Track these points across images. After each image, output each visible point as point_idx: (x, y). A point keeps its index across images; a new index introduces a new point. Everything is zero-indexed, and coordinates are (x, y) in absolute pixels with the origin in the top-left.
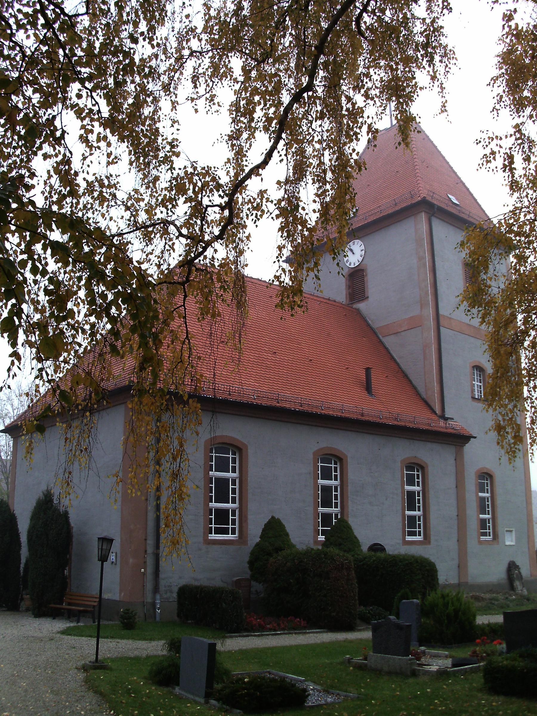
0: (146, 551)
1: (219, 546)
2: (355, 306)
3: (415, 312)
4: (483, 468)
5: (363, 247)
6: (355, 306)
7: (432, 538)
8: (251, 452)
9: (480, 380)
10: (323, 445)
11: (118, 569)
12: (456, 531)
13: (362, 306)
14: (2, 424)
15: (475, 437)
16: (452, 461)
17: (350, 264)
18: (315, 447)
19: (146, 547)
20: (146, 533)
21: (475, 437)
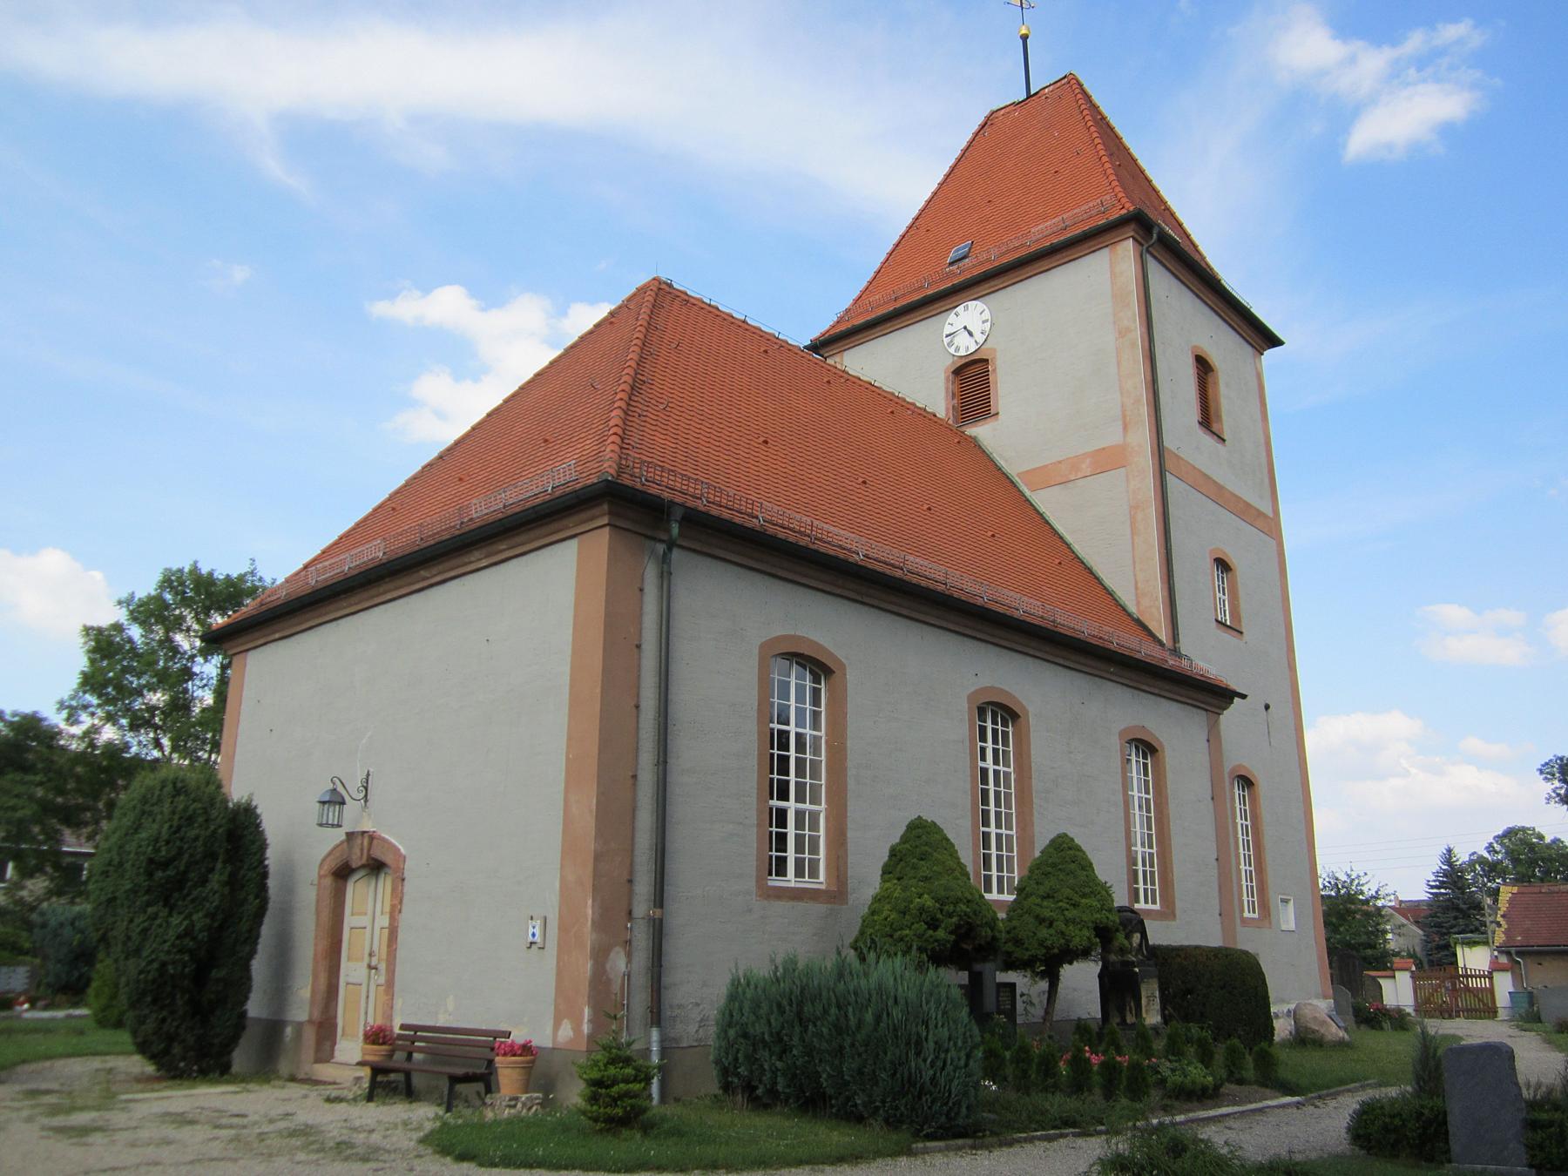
0: (630, 913)
1: (791, 903)
2: (972, 431)
3: (1113, 437)
4: (1240, 766)
5: (987, 315)
6: (972, 431)
7: (1178, 905)
8: (851, 676)
9: (816, 715)
10: (985, 681)
11: (550, 957)
12: (1216, 894)
13: (981, 431)
14: (549, 1030)
15: (1244, 697)
16: (1202, 744)
17: (957, 349)
18: (973, 684)
19: (630, 904)
20: (632, 865)
21: (1244, 697)
